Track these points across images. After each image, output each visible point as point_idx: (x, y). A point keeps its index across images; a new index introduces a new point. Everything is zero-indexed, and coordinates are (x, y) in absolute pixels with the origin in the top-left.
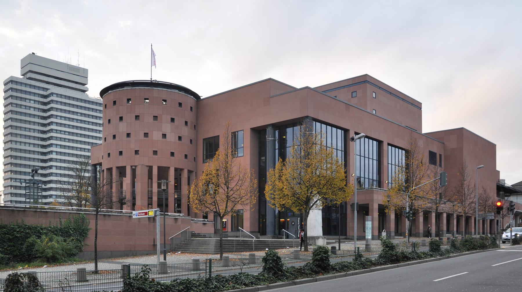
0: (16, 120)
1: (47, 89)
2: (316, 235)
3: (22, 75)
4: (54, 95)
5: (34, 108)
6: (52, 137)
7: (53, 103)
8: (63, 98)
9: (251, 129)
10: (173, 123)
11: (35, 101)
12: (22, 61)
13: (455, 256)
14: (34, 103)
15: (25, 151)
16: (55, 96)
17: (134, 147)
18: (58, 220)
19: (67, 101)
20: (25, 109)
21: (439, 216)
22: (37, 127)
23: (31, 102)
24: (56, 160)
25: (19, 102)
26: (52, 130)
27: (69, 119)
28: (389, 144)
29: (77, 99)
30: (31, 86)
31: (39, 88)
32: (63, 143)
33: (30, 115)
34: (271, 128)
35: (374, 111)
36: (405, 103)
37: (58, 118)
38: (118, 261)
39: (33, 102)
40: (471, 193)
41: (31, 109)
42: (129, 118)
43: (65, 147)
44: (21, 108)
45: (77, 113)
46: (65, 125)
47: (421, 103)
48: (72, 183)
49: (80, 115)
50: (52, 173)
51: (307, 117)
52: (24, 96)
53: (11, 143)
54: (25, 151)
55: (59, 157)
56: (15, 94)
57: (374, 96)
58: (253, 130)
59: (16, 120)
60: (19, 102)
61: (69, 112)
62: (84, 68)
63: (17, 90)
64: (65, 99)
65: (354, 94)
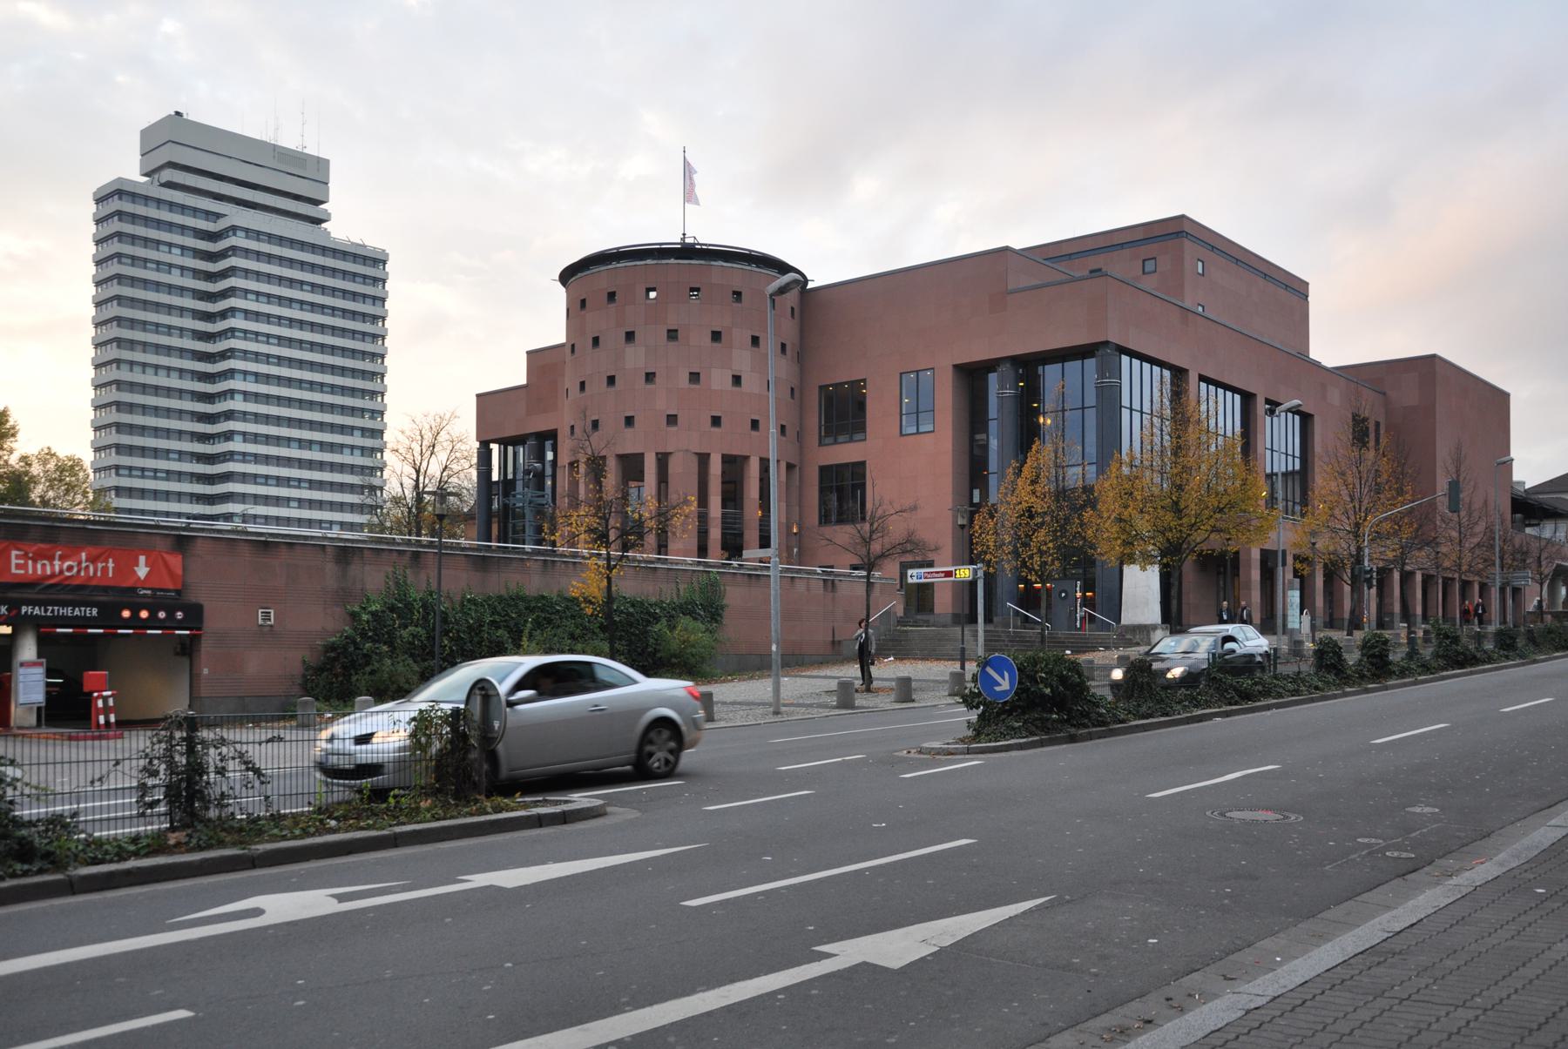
0: (133, 302)
1: (218, 216)
2: (1149, 622)
3: (146, 175)
4: (239, 233)
5: (182, 268)
6: (232, 350)
7: (234, 255)
8: (263, 241)
9: (955, 366)
10: (756, 349)
11: (183, 248)
12: (145, 134)
13: (1543, 661)
14: (182, 255)
15: (156, 390)
16: (242, 234)
17: (664, 405)
18: (673, 586)
19: (275, 250)
20: (158, 270)
21: (1407, 577)
22: (189, 323)
23: (174, 250)
24: (244, 416)
25: (140, 252)
26: (233, 330)
27: (281, 300)
28: (1202, 378)
29: (303, 245)
30: (172, 206)
31: (195, 211)
32: (263, 368)
33: (170, 288)
34: (1008, 365)
35: (1200, 309)
36: (1241, 269)
37: (250, 296)
38: (808, 673)
39: (178, 251)
40: (1476, 523)
41: (173, 270)
42: (651, 335)
43: (267, 379)
44: (145, 268)
45: (302, 283)
46: (268, 318)
47: (1308, 284)
48: (363, 487)
49: (309, 288)
50: (232, 453)
51: (1106, 343)
52: (153, 234)
53: (118, 368)
54: (156, 390)
55: (252, 407)
56: (128, 228)
57: (1200, 271)
58: (959, 368)
59: (133, 302)
60: (140, 252)
61: (281, 280)
62: (318, 158)
63: (134, 218)
64: (269, 243)
65: (1150, 266)
